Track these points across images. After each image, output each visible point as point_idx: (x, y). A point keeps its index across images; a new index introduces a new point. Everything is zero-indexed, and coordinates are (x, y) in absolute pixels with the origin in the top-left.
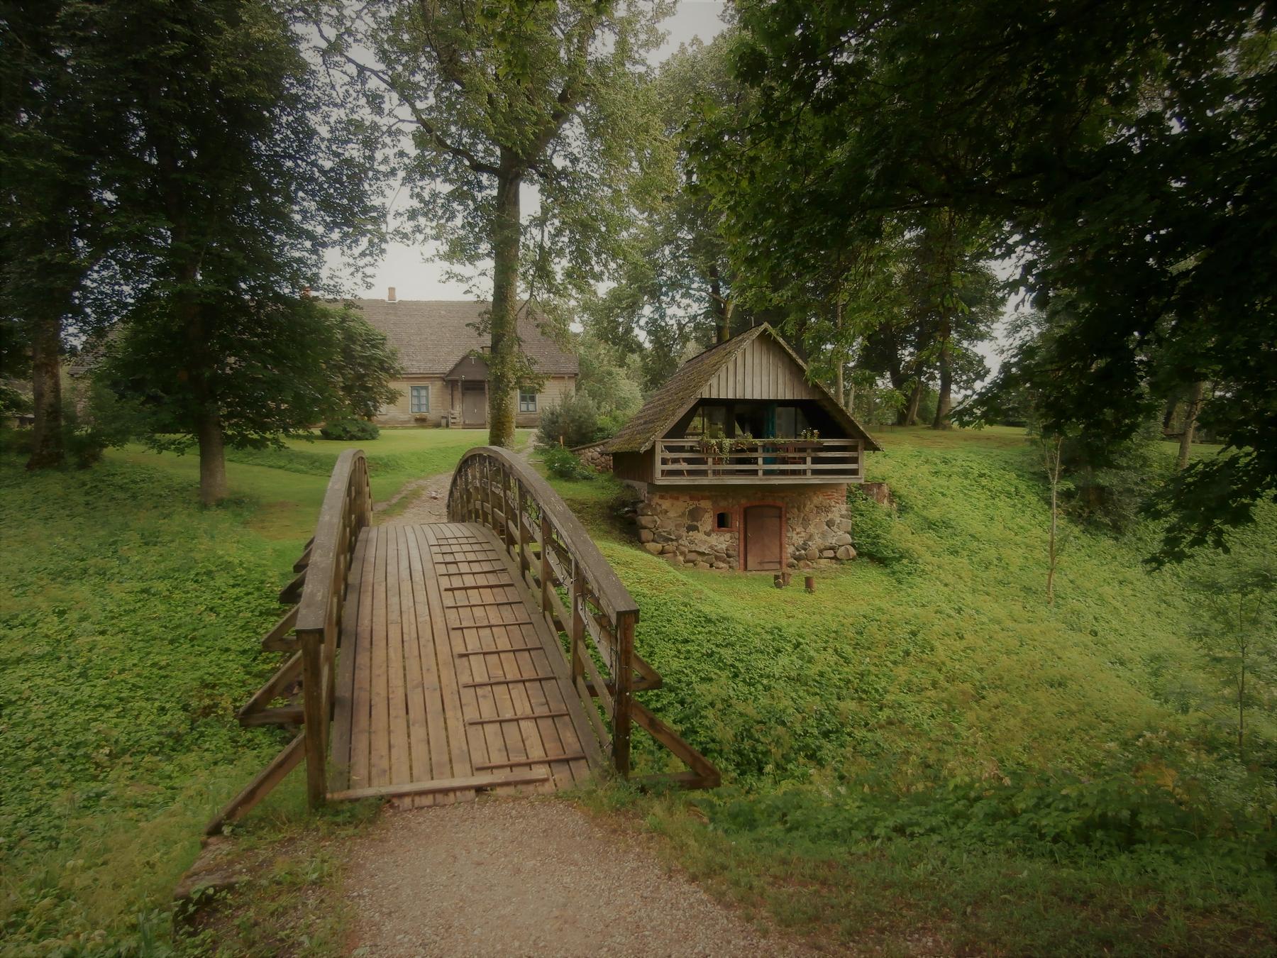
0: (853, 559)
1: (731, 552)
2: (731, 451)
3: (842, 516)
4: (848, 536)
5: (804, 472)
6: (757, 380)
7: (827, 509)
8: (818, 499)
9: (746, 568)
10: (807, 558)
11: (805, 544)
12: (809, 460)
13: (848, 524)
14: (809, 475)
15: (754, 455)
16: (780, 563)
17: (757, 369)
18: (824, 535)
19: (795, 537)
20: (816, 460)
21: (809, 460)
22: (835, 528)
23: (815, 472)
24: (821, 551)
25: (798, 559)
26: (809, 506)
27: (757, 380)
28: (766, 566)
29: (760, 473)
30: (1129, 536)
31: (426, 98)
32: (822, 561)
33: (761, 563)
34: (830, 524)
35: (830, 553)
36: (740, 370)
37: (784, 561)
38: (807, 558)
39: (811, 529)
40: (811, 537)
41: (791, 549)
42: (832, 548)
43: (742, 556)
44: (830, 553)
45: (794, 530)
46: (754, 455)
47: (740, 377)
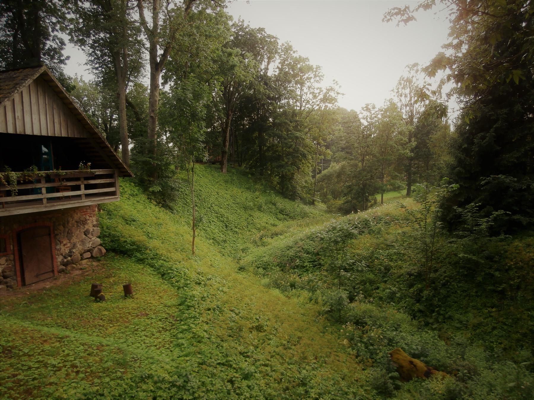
0: (105, 255)
1: (8, 273)
2: (19, 183)
3: (94, 226)
4: (99, 240)
5: (79, 196)
6: (35, 117)
7: (84, 222)
8: (76, 217)
9: (24, 284)
10: (72, 262)
11: (70, 252)
12: (83, 186)
13: (98, 230)
14: (84, 197)
15: (38, 186)
16: (53, 271)
17: (35, 108)
18: (83, 242)
19: (63, 248)
20: (88, 187)
21: (83, 186)
22: (90, 236)
23: (88, 196)
24: (81, 255)
25: (65, 264)
26: (72, 222)
27: (35, 117)
28: (42, 277)
29: (45, 201)
30: (178, 205)
31: (207, 107)
32: (84, 262)
33: (37, 276)
34: (86, 233)
35: (88, 255)
36: (18, 108)
37: (56, 269)
38: (72, 262)
39: (74, 240)
40: (74, 246)
41: (60, 259)
42: (88, 251)
43: (19, 273)
44: (88, 255)
45: (61, 242)
46: (38, 186)
47: (18, 114)
